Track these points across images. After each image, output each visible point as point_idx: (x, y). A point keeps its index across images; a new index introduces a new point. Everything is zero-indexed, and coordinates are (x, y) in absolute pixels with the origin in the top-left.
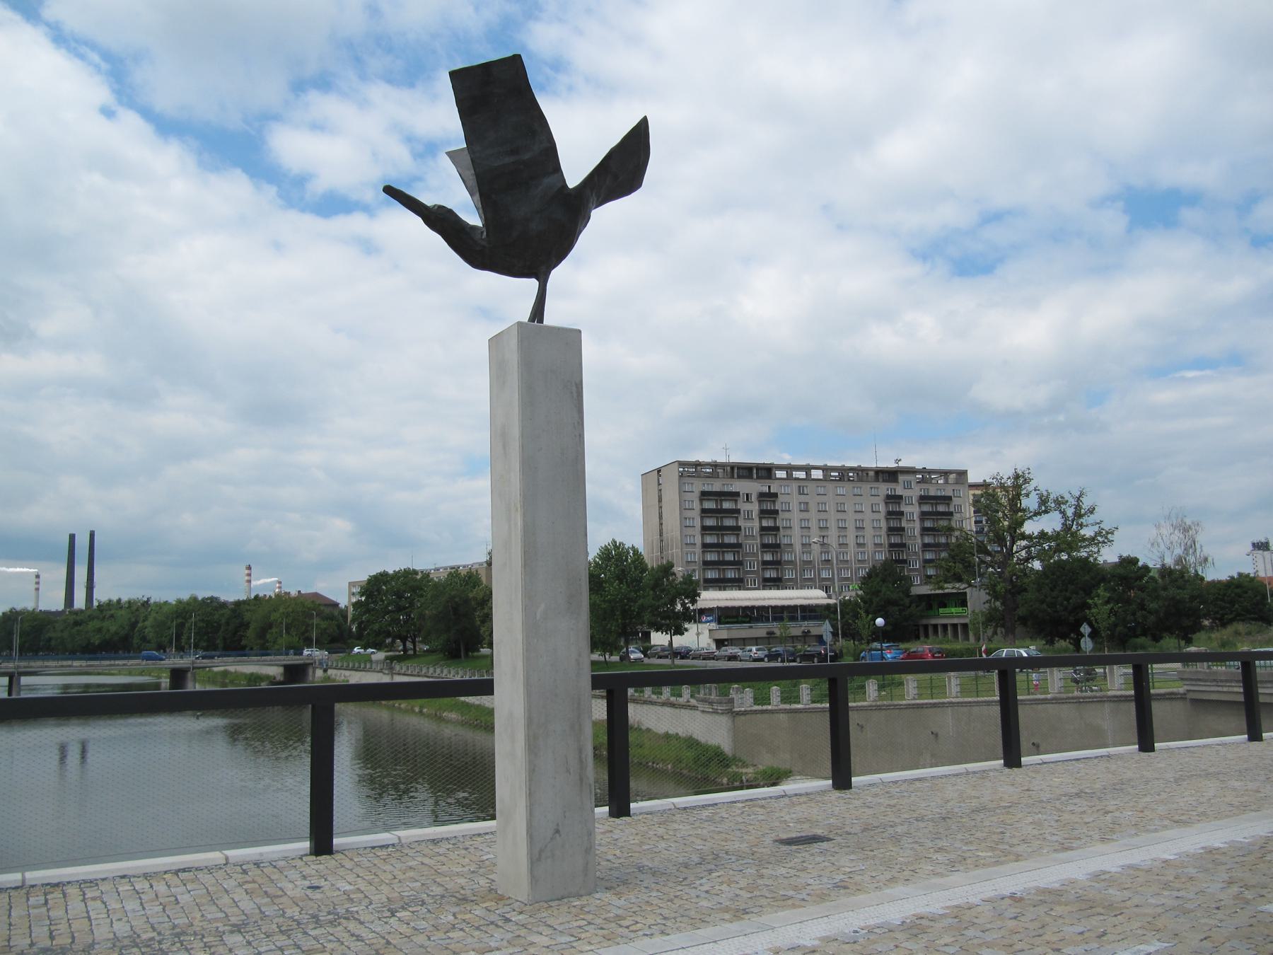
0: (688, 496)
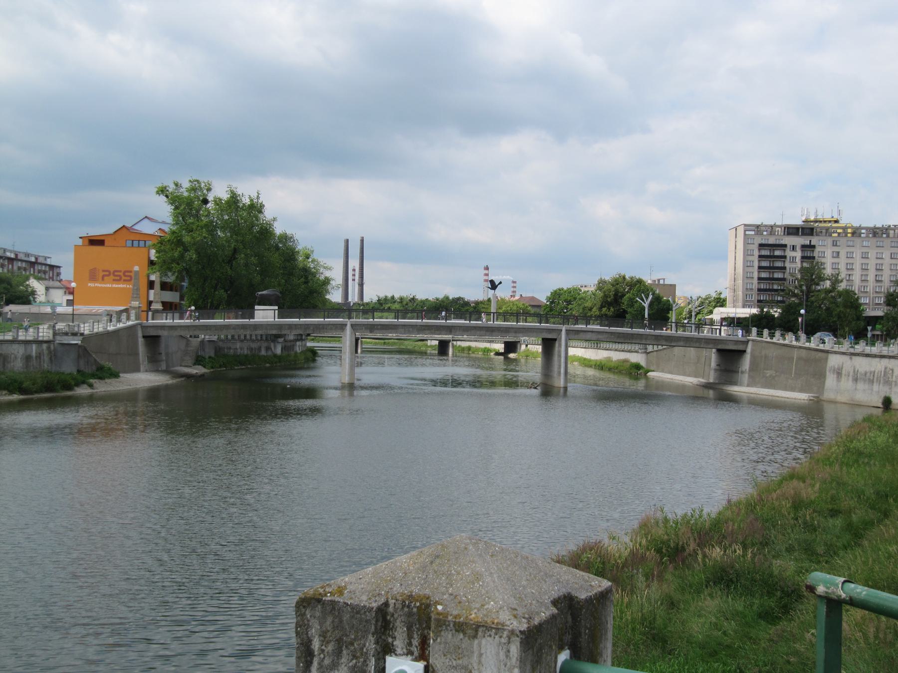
0: (751, 247)
